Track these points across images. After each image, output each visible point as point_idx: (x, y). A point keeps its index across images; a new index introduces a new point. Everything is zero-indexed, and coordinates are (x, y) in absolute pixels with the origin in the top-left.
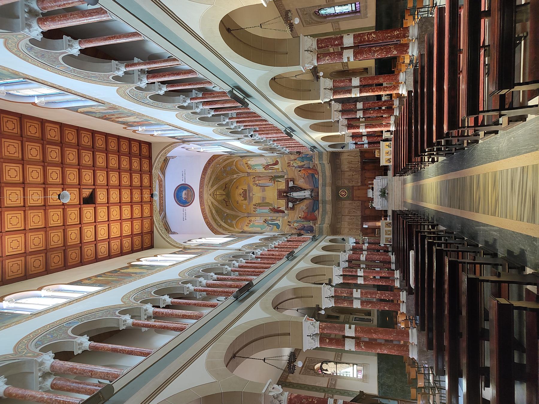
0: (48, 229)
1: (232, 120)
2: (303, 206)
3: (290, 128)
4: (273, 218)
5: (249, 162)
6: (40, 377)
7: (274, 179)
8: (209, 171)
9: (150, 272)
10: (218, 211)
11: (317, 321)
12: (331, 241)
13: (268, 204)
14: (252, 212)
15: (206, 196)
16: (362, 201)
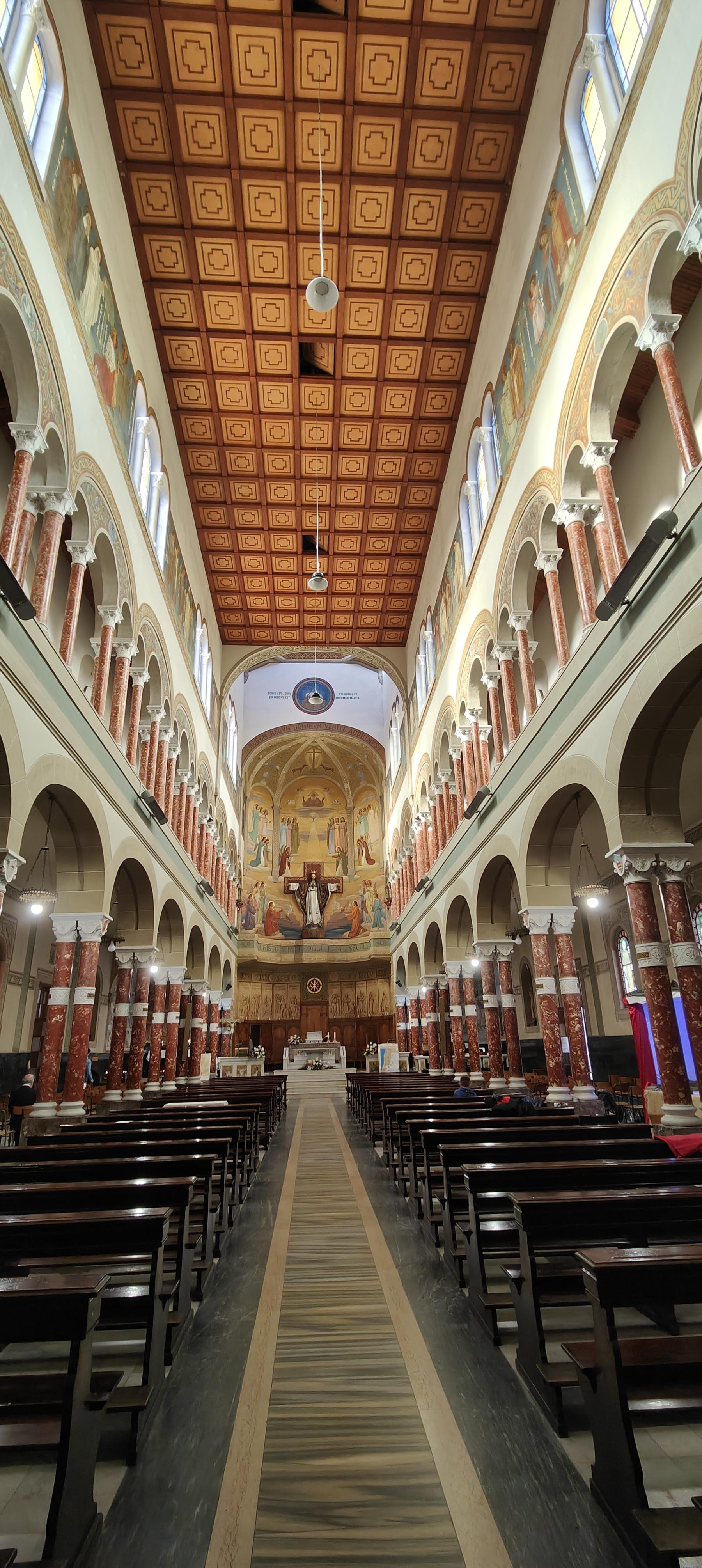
0: (261, 480)
1: (444, 787)
2: (291, 910)
3: (431, 888)
4: (270, 855)
5: (371, 811)
6: (38, 494)
7: (342, 856)
8: (356, 741)
9: (185, 644)
10: (283, 757)
11: (103, 938)
12: (227, 963)
13: (296, 844)
14: (282, 816)
15: (312, 734)
16: (299, 1021)
